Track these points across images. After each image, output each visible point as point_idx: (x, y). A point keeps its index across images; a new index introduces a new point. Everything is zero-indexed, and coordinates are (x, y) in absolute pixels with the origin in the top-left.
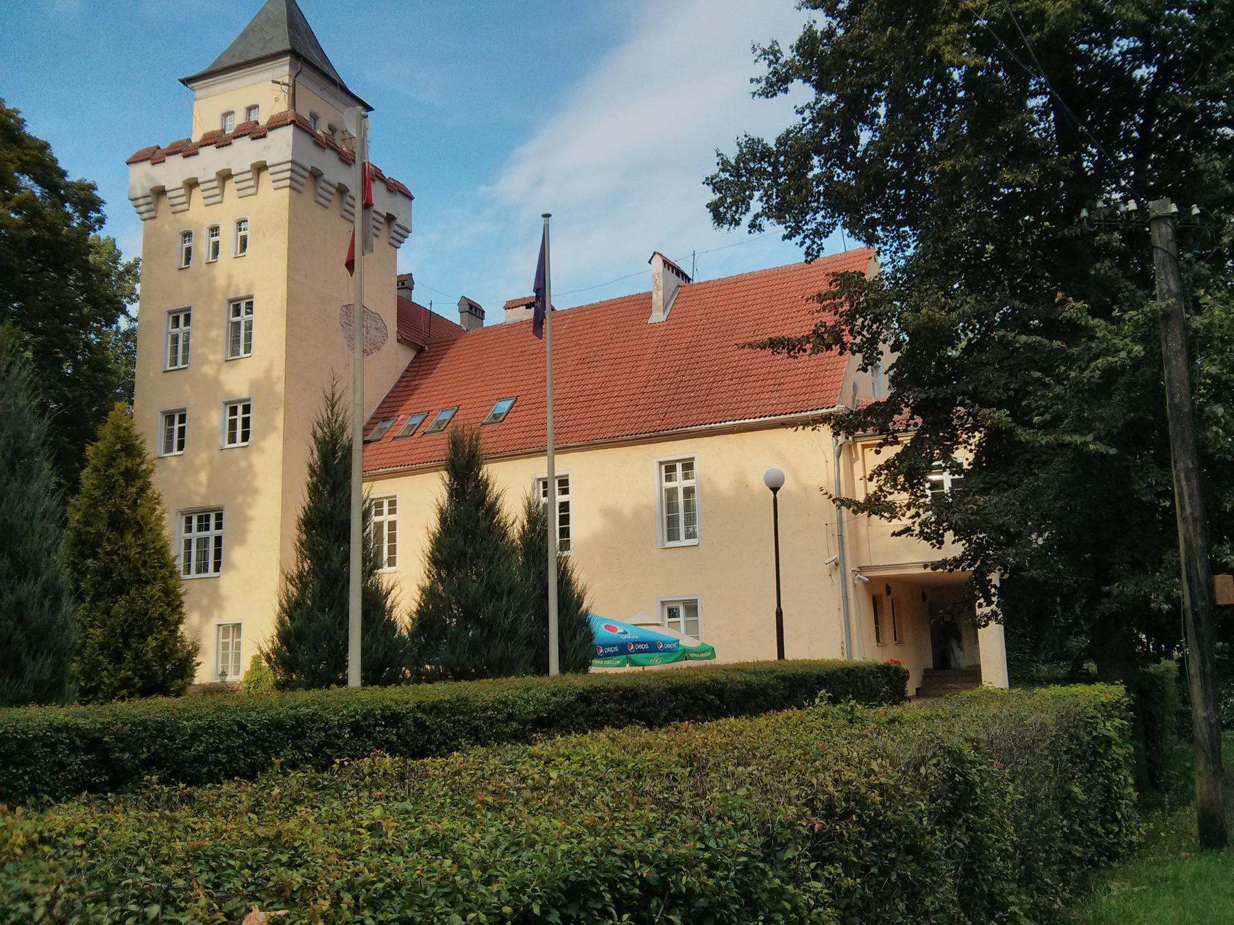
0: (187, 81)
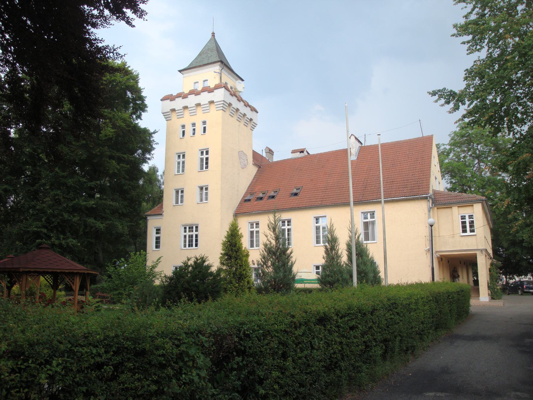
0: (180, 71)
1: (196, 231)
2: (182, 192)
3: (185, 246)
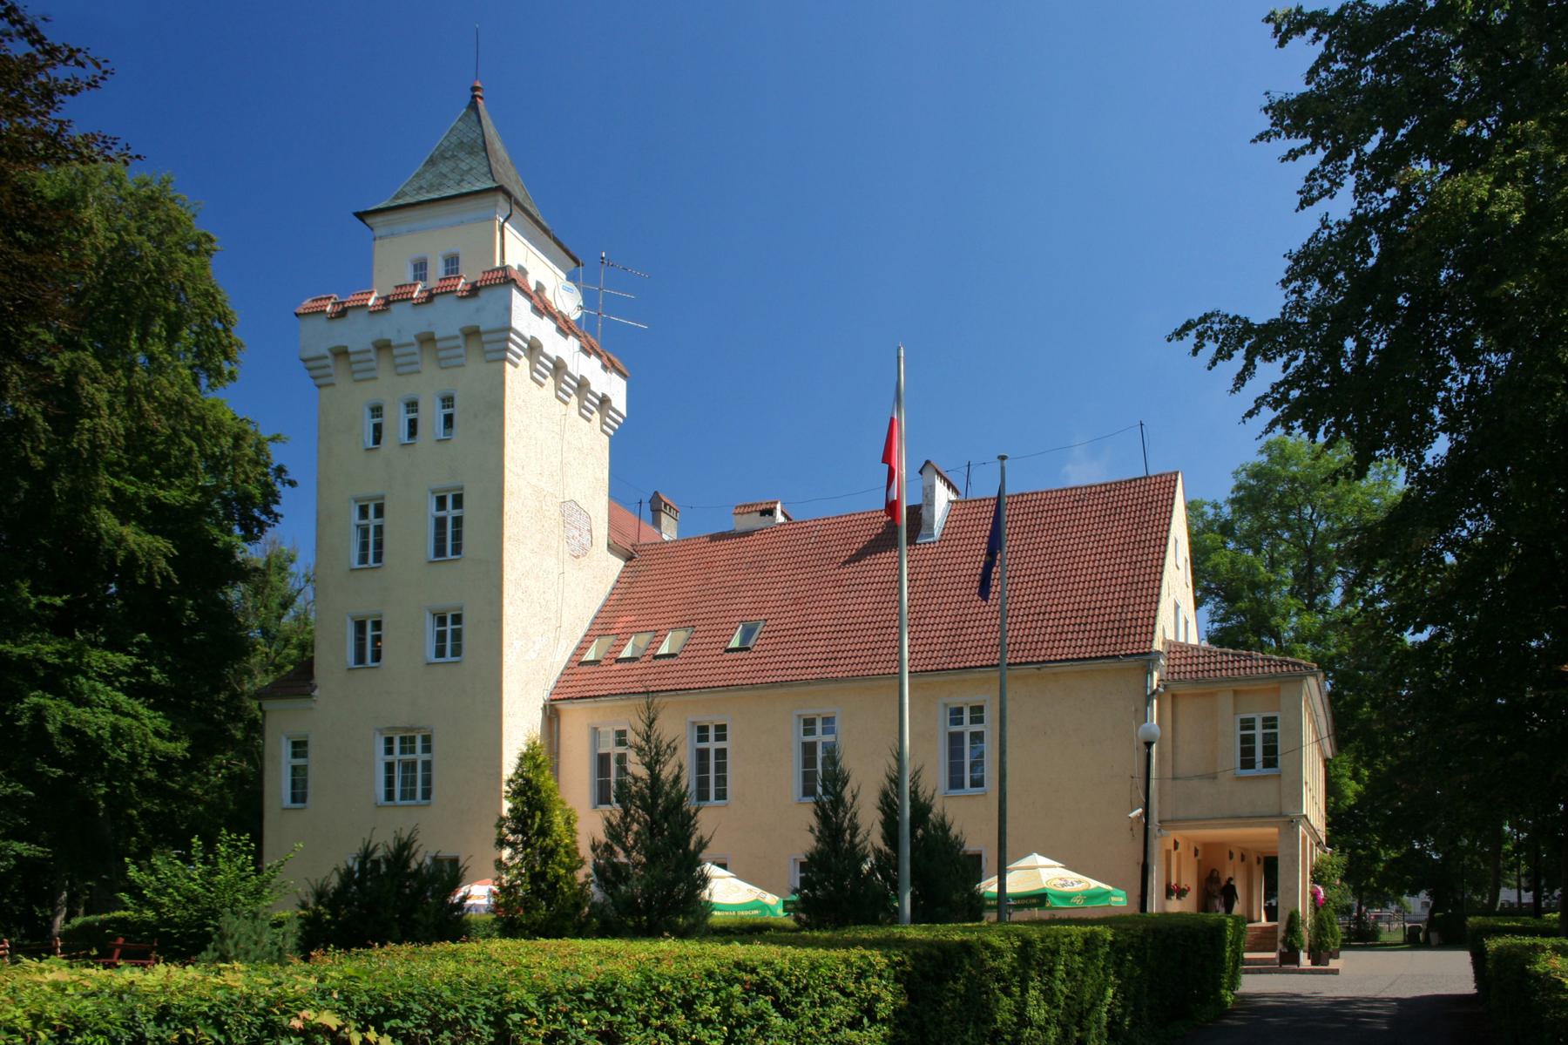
2: (377, 625)
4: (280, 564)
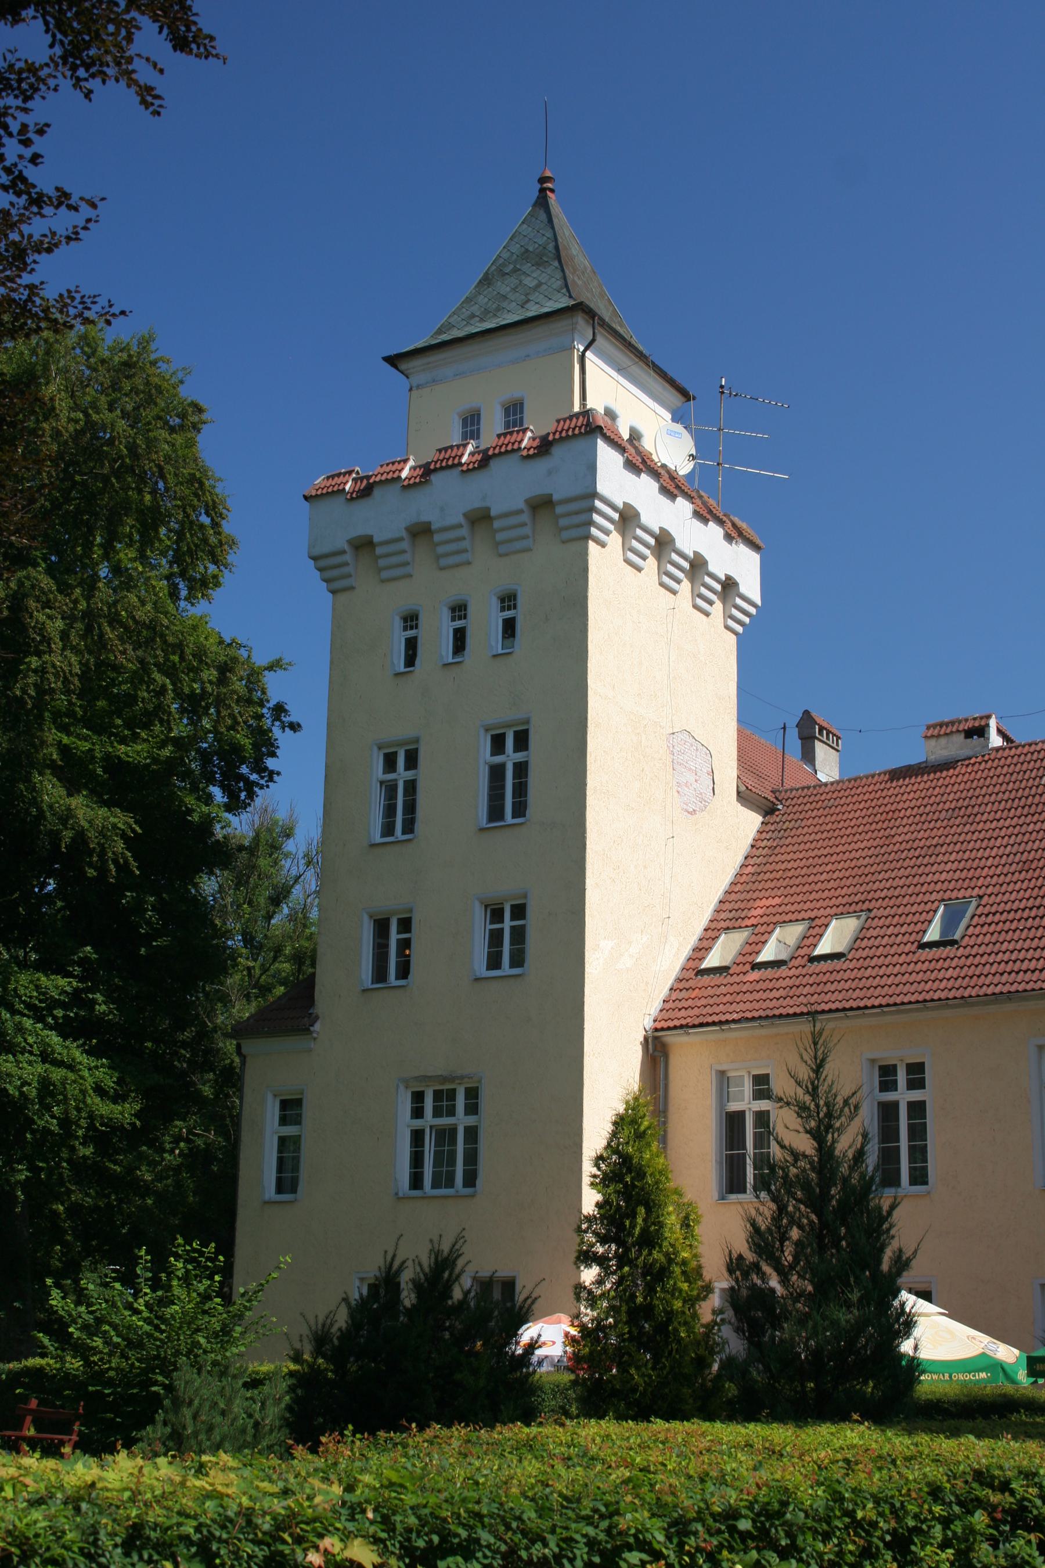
1: (472, 1108)
2: (405, 925)
3: (416, 1182)
4: (271, 840)
